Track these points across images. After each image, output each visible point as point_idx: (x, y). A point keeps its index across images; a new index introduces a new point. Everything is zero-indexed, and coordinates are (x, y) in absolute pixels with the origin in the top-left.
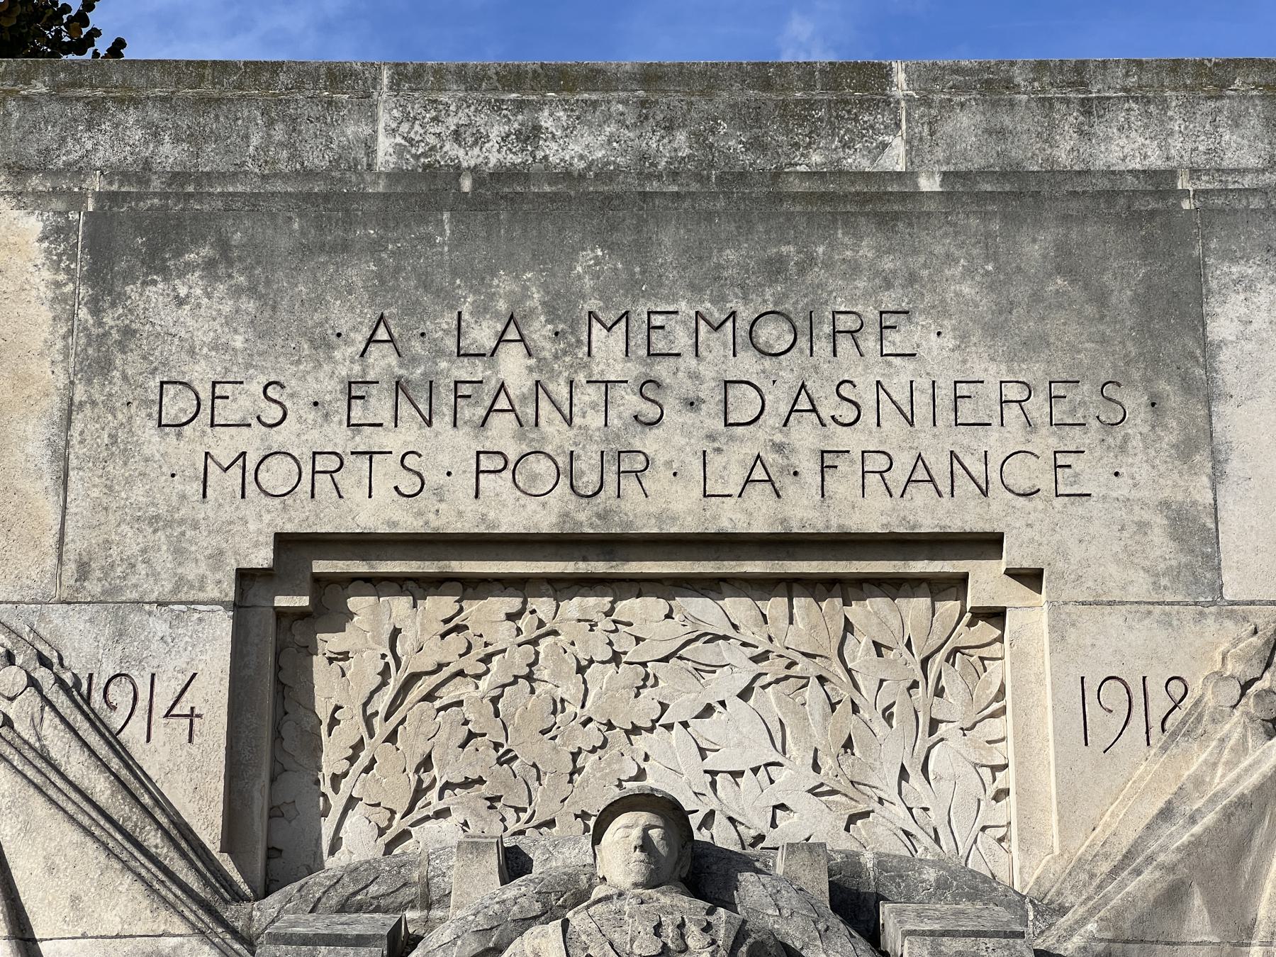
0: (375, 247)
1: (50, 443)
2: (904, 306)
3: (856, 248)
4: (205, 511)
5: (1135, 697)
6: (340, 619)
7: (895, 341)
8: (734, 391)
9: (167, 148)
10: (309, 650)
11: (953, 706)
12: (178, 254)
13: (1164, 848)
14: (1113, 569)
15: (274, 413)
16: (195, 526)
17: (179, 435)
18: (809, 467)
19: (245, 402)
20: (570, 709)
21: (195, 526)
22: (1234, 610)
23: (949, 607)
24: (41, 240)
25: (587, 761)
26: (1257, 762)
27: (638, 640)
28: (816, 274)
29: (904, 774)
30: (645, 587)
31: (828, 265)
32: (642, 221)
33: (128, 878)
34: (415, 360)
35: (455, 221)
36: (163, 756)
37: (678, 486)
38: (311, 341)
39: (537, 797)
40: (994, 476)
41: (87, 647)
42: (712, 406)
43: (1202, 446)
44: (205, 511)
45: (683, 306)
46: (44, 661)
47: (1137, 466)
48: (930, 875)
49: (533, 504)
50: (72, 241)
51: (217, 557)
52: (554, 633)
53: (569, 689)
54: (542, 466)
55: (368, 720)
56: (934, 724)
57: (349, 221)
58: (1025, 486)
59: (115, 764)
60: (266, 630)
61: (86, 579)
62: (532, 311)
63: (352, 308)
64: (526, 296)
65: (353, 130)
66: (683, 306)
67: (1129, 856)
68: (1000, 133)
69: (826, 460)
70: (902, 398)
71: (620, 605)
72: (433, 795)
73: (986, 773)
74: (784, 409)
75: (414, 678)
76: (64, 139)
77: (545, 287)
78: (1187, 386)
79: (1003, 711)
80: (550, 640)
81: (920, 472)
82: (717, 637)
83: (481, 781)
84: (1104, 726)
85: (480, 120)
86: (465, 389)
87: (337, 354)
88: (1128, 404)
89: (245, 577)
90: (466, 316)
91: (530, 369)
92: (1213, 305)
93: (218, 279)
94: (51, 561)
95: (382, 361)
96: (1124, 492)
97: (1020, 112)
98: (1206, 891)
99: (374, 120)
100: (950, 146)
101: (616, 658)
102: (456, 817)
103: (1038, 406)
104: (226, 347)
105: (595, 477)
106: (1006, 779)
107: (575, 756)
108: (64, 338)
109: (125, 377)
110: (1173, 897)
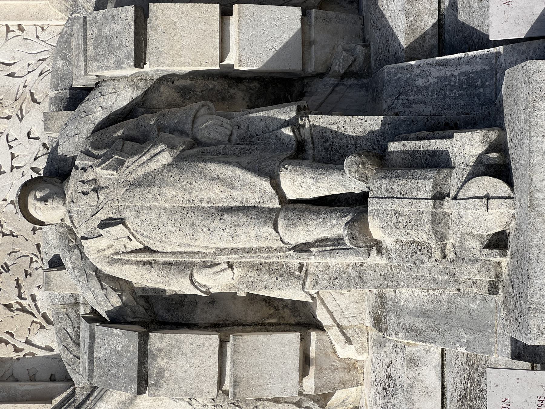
29: (11, 75)
39: (25, 253)
48: (60, 63)
73: (10, 35)
83: (17, 280)
102: (35, 291)
106: (13, 26)
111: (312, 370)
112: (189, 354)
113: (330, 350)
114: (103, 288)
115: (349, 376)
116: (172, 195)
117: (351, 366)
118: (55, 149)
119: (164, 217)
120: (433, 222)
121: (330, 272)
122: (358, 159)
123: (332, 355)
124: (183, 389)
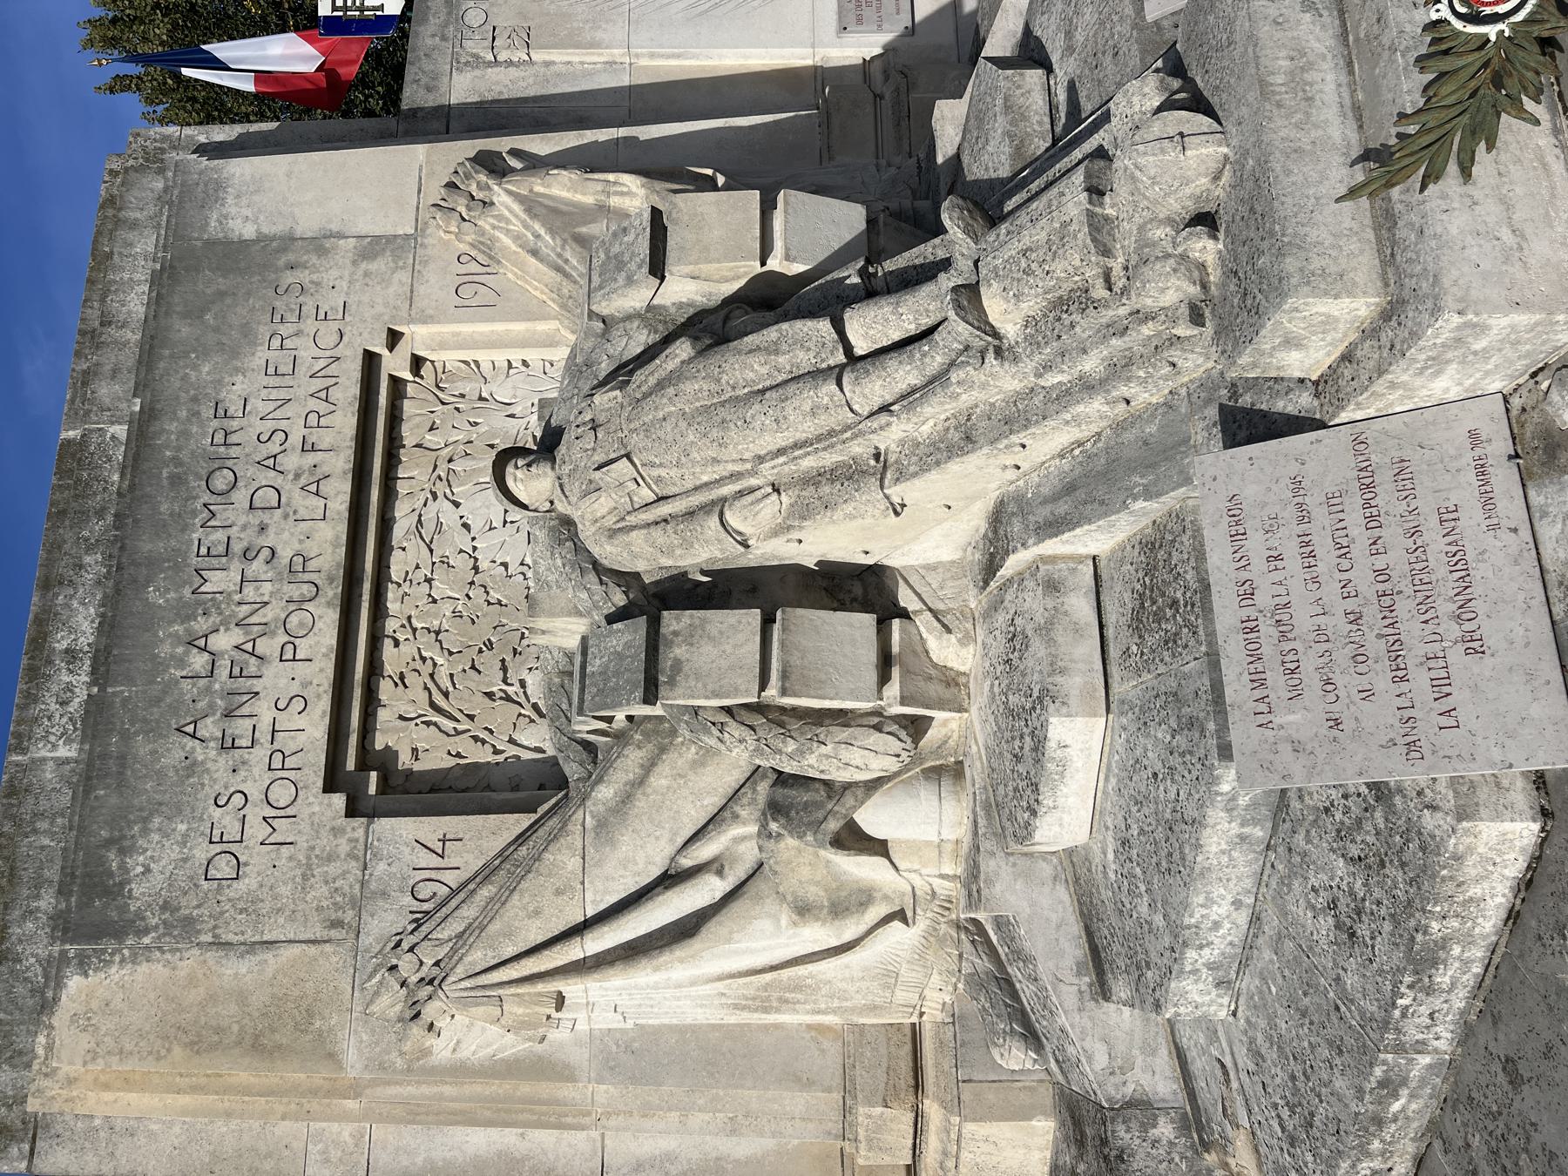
0: (126, 737)
1: (242, 956)
2: (212, 404)
3: (170, 432)
4: (303, 843)
5: (468, 280)
6: (390, 754)
7: (235, 408)
8: (257, 503)
9: (42, 904)
10: (409, 773)
11: (468, 388)
12: (111, 875)
13: (553, 249)
14: (391, 290)
15: (238, 800)
16: (313, 848)
17: (246, 864)
18: (311, 458)
19: (227, 820)
20: (460, 608)
21: (313, 848)
22: (420, 229)
23: (410, 389)
24: (87, 976)
25: (494, 596)
26: (508, 208)
27: (418, 567)
28: (184, 456)
29: (512, 416)
30: (384, 564)
31: (179, 449)
32: (134, 563)
33: (546, 855)
34: (212, 706)
35: (116, 683)
36: (470, 857)
37: (316, 536)
38: (188, 777)
39: (515, 625)
40: (328, 353)
41: (390, 916)
42: (265, 517)
43: (320, 244)
44: (303, 843)
45: (195, 536)
46: (398, 944)
47: (329, 277)
49: (319, 624)
50: (90, 952)
51: (336, 832)
52: (409, 618)
53: (447, 608)
54: (294, 620)
55: (458, 733)
56: (481, 399)
57: (104, 756)
58: (336, 337)
59: (472, 886)
60: (390, 800)
61: (342, 923)
62: (186, 630)
63: (168, 750)
64: (176, 635)
65: (49, 773)
66: (195, 536)
67: (558, 269)
68: (115, 372)
69: (307, 447)
70: (272, 405)
71: (394, 578)
72: (510, 690)
74: (272, 473)
75: (433, 705)
76: (25, 979)
77: (171, 623)
78: (283, 250)
79: (476, 362)
80: (414, 621)
81: (324, 395)
82: (419, 521)
83: (503, 661)
84: (485, 295)
85: (55, 688)
86: (236, 671)
87: (200, 758)
88: (290, 280)
89: (351, 812)
90: (184, 673)
91: (227, 630)
92: (235, 236)
93: (134, 845)
94: (328, 948)
95: (209, 728)
96: (345, 284)
97: (103, 360)
98: (577, 225)
99: (44, 759)
100: (119, 399)
101: (429, 581)
102: (525, 675)
103: (284, 330)
104: (185, 836)
105: (305, 586)
107: (489, 603)
108: (163, 952)
109: (198, 906)
110: (582, 241)
111: (896, 672)
112: (719, 647)
113: (919, 649)
114: (601, 583)
115: (947, 694)
116: (696, 390)
117: (951, 680)
118: (548, 422)
119: (683, 425)
120: (1090, 225)
121: (922, 450)
122: (960, 202)
123: (923, 656)
124: (710, 687)
